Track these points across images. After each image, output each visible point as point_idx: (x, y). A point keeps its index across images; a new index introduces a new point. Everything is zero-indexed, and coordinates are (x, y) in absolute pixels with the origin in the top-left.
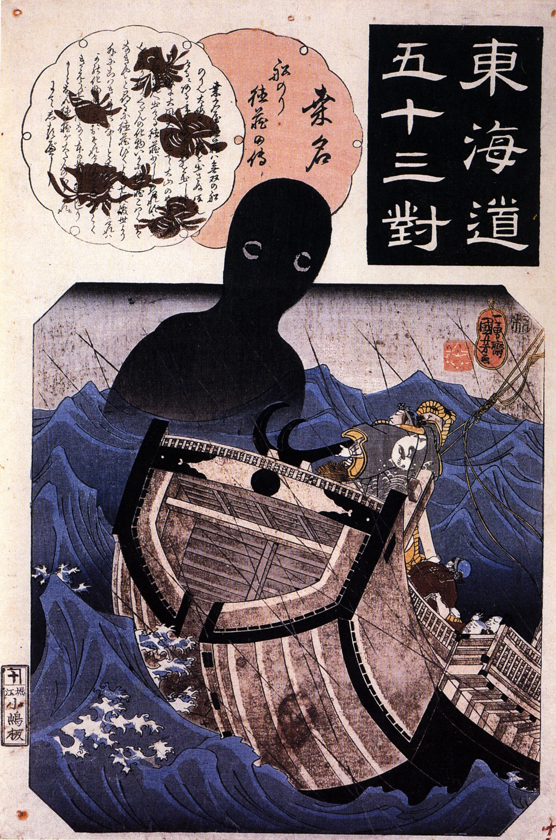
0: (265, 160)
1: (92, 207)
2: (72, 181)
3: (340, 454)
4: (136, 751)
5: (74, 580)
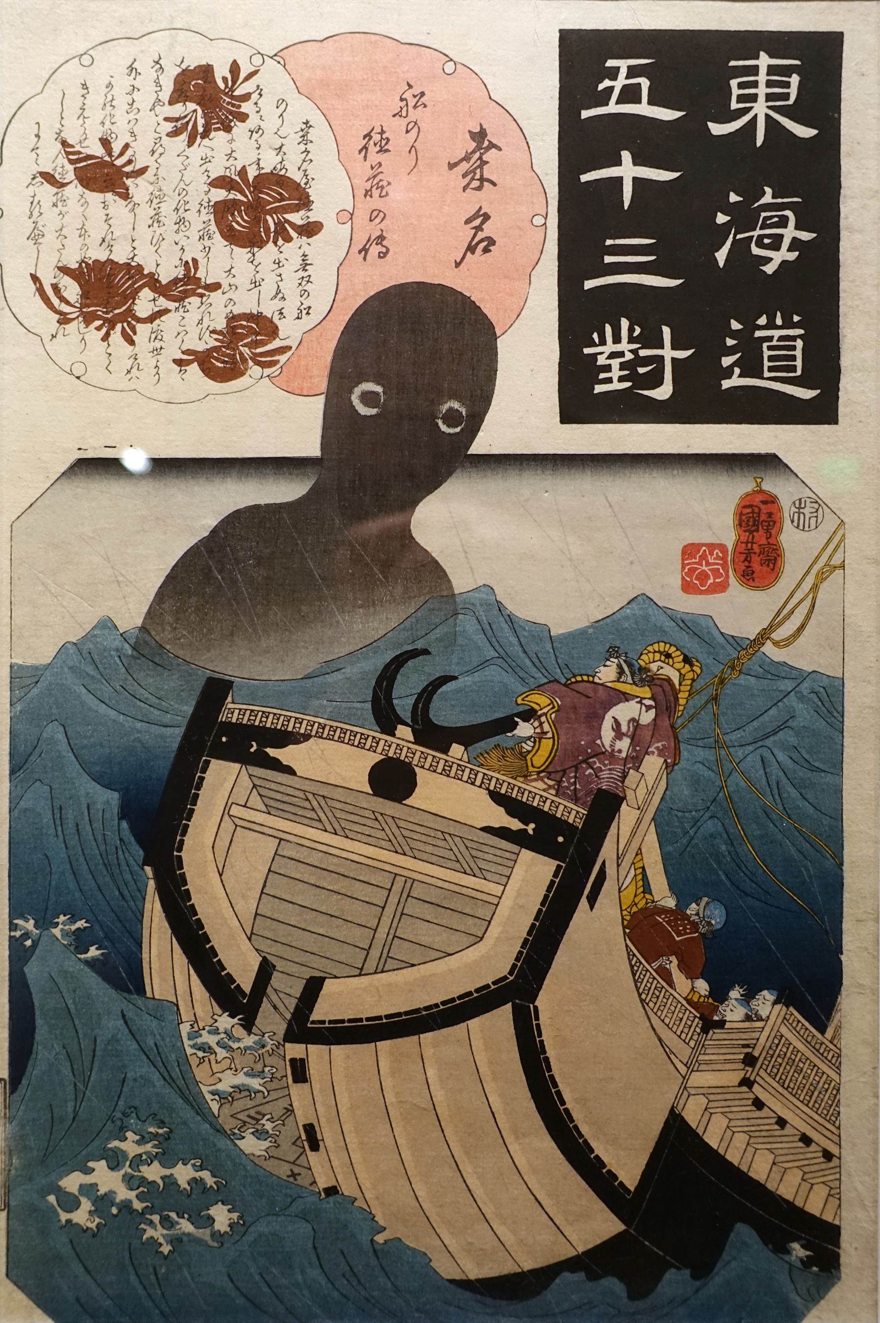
0: (388, 250)
1: (104, 330)
2: (72, 290)
3: (514, 732)
4: (181, 1221)
5: (80, 942)
